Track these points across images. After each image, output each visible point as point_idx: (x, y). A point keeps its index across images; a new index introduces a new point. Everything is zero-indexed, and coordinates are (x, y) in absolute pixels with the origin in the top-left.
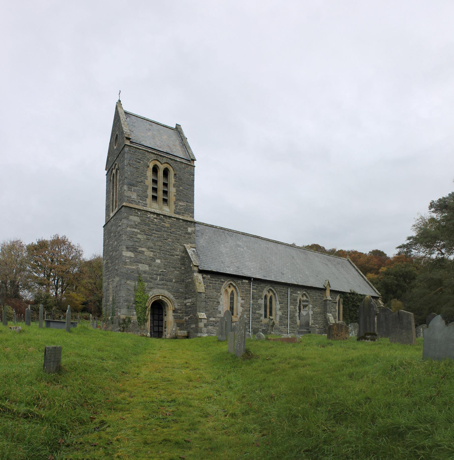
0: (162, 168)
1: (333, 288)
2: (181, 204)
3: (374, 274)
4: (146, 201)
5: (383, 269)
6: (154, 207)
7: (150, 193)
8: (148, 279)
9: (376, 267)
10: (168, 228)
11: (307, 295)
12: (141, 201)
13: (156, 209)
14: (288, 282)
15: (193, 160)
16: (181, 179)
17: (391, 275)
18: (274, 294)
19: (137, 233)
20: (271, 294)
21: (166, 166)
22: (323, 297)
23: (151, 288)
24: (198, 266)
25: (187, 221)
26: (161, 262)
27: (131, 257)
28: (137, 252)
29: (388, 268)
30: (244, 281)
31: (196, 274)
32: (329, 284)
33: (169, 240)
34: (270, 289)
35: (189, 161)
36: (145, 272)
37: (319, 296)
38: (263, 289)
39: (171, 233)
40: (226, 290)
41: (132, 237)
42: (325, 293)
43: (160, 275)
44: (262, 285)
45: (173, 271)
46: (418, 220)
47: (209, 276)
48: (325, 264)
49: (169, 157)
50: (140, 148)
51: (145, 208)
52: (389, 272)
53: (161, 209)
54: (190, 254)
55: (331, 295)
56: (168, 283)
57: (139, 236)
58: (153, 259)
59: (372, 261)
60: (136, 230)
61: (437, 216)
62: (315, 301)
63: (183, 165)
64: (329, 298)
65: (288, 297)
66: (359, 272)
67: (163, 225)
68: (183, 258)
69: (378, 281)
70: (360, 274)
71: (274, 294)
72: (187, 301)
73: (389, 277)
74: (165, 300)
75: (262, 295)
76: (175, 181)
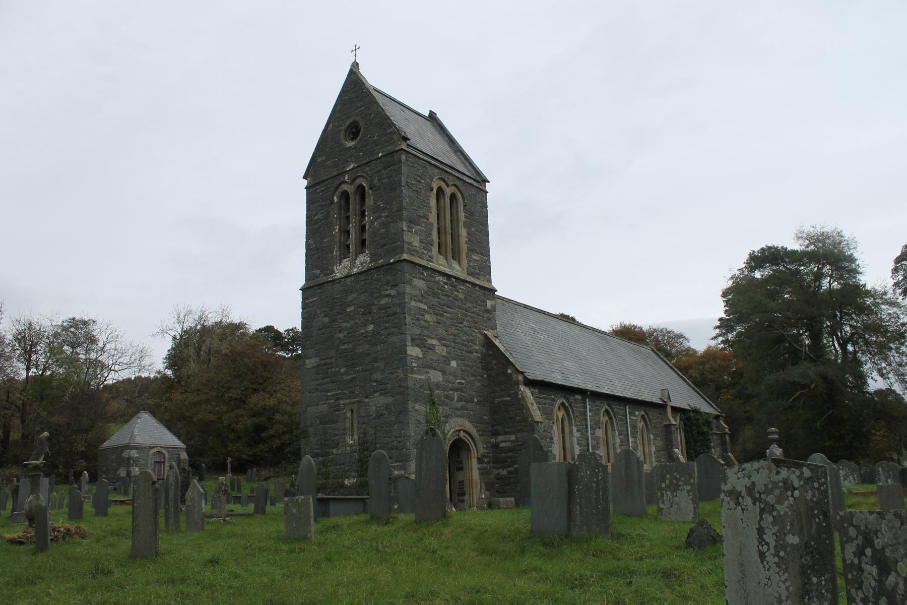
0: (448, 191)
2: (474, 257)
8: (443, 399)
10: (462, 301)
12: (425, 252)
16: (472, 214)
23: (447, 417)
24: (522, 373)
26: (458, 365)
28: (425, 347)
31: (522, 388)
36: (438, 386)
41: (418, 319)
42: (666, 412)
43: (457, 390)
47: (537, 390)
53: (450, 266)
56: (469, 406)
57: (427, 317)
60: (422, 306)
65: (627, 423)
67: (456, 295)
71: (611, 418)
72: (500, 438)
76: (466, 217)
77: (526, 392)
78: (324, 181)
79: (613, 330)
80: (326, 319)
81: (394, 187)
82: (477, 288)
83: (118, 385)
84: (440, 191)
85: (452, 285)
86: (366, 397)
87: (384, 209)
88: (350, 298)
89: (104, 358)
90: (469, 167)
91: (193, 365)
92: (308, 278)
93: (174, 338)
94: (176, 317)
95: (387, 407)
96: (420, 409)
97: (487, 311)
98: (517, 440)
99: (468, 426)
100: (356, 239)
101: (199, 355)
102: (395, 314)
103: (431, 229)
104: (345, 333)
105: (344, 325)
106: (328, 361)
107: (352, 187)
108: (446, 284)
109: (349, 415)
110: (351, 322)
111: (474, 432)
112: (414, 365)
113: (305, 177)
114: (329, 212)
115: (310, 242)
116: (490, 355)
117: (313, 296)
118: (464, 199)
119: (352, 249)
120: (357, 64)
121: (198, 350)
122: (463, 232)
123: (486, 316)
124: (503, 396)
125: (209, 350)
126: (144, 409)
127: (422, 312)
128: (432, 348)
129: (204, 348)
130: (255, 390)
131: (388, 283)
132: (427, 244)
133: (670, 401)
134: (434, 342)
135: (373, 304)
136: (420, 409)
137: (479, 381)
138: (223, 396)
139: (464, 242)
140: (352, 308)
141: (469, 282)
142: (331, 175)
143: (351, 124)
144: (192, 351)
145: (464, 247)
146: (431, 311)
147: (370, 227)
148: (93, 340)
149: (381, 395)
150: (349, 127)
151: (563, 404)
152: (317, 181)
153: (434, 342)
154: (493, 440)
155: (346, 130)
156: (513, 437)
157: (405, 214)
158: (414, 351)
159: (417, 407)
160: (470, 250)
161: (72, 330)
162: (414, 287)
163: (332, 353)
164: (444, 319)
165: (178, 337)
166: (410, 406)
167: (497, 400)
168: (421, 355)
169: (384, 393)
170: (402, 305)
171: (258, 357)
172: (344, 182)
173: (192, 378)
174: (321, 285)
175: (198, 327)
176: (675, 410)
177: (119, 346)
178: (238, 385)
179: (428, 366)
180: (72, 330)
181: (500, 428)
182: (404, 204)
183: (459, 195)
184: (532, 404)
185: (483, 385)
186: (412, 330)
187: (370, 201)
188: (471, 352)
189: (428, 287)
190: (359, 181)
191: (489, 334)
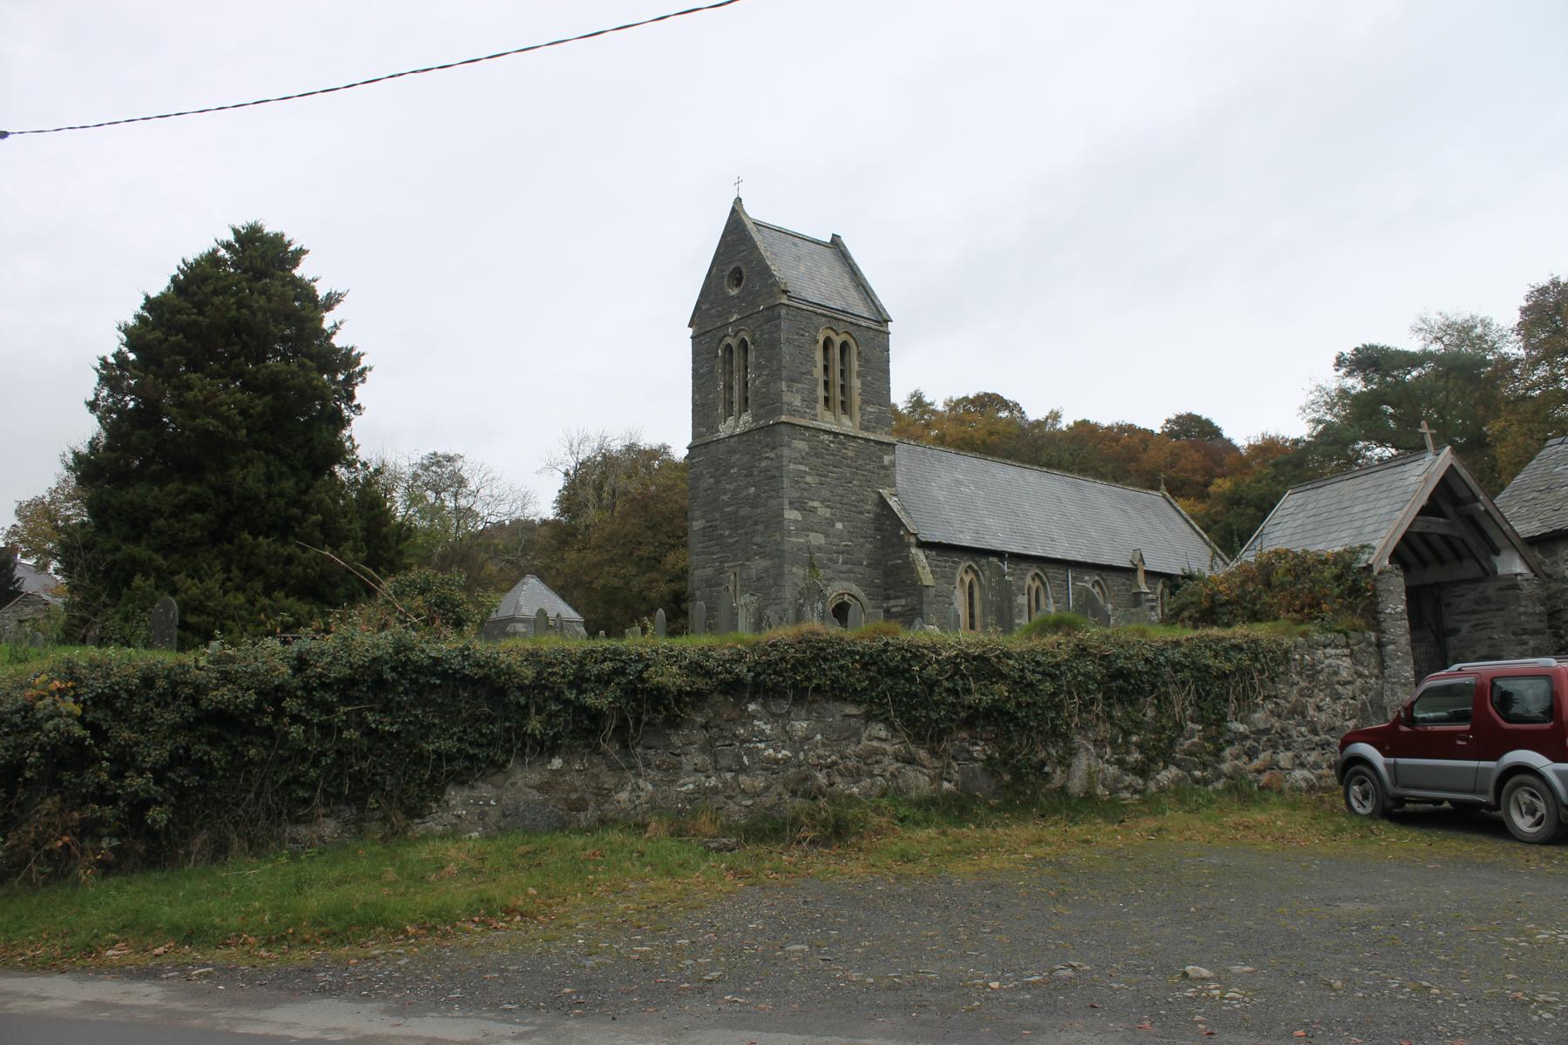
0: (838, 340)
1: (1149, 567)
2: (869, 410)
3: (1196, 499)
4: (815, 408)
5: (1222, 485)
6: (827, 421)
7: (821, 393)
9: (1199, 478)
10: (851, 459)
11: (1102, 582)
12: (808, 411)
13: (831, 424)
14: (1069, 558)
15: (887, 321)
16: (868, 361)
17: (1248, 505)
18: (1044, 584)
19: (805, 472)
20: (1038, 583)
21: (844, 337)
22: (1131, 586)
23: (829, 580)
24: (915, 535)
25: (882, 443)
26: (844, 526)
27: (797, 521)
28: (805, 510)
29: (1236, 484)
30: (991, 559)
31: (913, 550)
32: (1142, 559)
33: (855, 482)
34: (1037, 574)
35: (879, 322)
36: (819, 549)
37: (1123, 584)
38: (1025, 574)
39: (857, 469)
40: (962, 579)
41: (797, 482)
42: (1135, 577)
43: (843, 552)
44: (1023, 566)
45: (862, 545)
46: (1311, 392)
48: (1122, 510)
49: (849, 320)
50: (804, 307)
51: (815, 424)
52: (1241, 497)
53: (838, 422)
54: (896, 510)
55: (1146, 582)
56: (857, 569)
57: (808, 479)
58: (831, 523)
59: (1186, 458)
60: (803, 468)
61: (1356, 384)
62: (1118, 595)
63: (872, 333)
64: (1144, 589)
65: (1068, 589)
66: (1191, 526)
67: (844, 454)
68: (877, 517)
69: (1210, 523)
70: (1194, 529)
71: (1044, 584)
72: (892, 603)
73: (1240, 511)
74: (852, 602)
75: (1024, 586)
76: (860, 366)
77: (919, 555)
78: (708, 332)
79: (1250, 445)
80: (712, 480)
81: (774, 344)
82: (872, 444)
83: (147, 415)
84: (828, 343)
85: (840, 443)
86: (748, 560)
87: (766, 366)
88: (733, 459)
89: (477, 508)
90: (871, 304)
91: (592, 511)
92: (694, 437)
93: (567, 474)
94: (568, 445)
95: (766, 570)
96: (798, 573)
97: (884, 468)
98: (906, 605)
99: (855, 589)
100: (739, 397)
101: (600, 498)
102: (774, 477)
103: (817, 385)
104: (729, 495)
105: (728, 486)
106: (713, 523)
107: (735, 341)
108: (831, 442)
109: (732, 577)
110: (735, 484)
111: (862, 595)
112: (792, 528)
113: (690, 325)
114: (713, 367)
115: (696, 397)
116: (884, 515)
117: (699, 455)
118: (858, 346)
119: (736, 408)
120: (740, 199)
121: (599, 488)
122: (856, 383)
123: (882, 472)
124: (896, 559)
125: (614, 492)
126: (530, 573)
127: (802, 474)
128: (813, 510)
129: (606, 488)
130: (673, 546)
131: (767, 446)
132: (810, 402)
133: (1144, 564)
134: (816, 504)
135: (754, 466)
136: (798, 573)
137: (870, 543)
138: (631, 554)
139: (856, 394)
140: (735, 470)
141: (861, 438)
142: (716, 326)
143: (735, 269)
144: (590, 491)
145: (856, 399)
146: (813, 472)
147: (752, 385)
148: (462, 482)
149: (761, 558)
150: (731, 273)
151: (970, 567)
152: (702, 331)
153: (816, 504)
154: (885, 605)
155: (729, 277)
156: (903, 602)
157: (784, 373)
158: (791, 515)
159: (794, 570)
160: (865, 402)
161: (434, 468)
162: (794, 449)
163: (717, 515)
164: (828, 480)
165: (572, 472)
166: (787, 568)
167: (890, 563)
168: (800, 519)
169: (763, 556)
170: (780, 468)
171: (676, 502)
172: (727, 335)
173: (591, 529)
174: (707, 445)
175: (599, 459)
176: (1151, 575)
177: (496, 492)
178: (651, 540)
179: (806, 528)
180: (434, 468)
181: (891, 592)
182: (784, 362)
183: (852, 342)
184: (924, 568)
185: (875, 547)
186: (789, 491)
187: (752, 358)
188: (861, 513)
189: (810, 448)
190: (742, 334)
191: (885, 492)
